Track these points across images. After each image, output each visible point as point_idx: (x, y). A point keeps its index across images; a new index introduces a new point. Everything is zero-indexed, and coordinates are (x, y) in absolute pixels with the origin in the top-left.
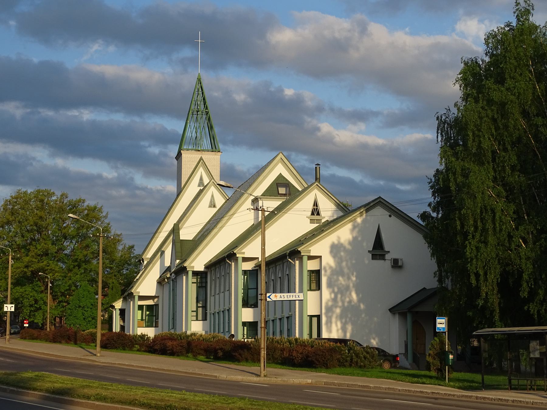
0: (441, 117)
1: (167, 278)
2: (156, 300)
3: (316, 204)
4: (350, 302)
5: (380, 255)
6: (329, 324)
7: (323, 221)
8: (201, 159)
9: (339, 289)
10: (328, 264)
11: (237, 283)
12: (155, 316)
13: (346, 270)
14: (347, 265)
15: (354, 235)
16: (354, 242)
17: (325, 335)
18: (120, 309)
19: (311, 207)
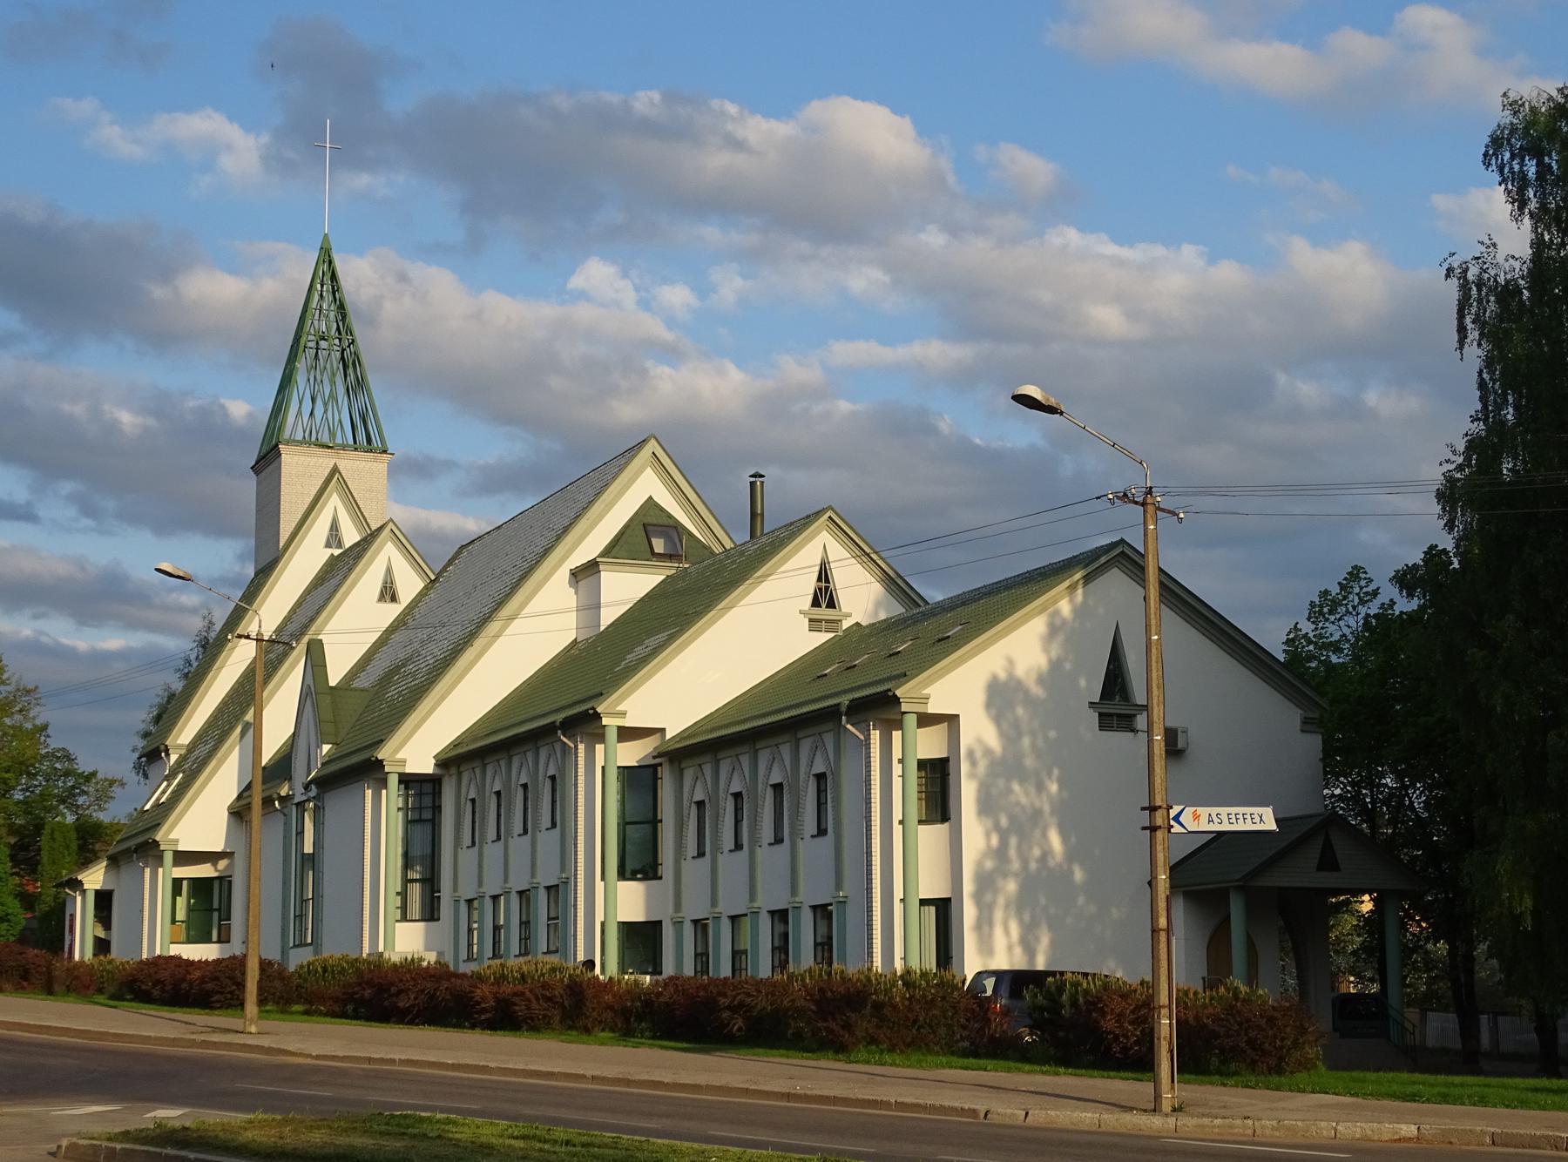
0: (1466, 271)
1: (282, 799)
2: (222, 864)
3: (824, 575)
4: (1046, 855)
5: (1119, 715)
6: (986, 928)
7: (846, 624)
8: (335, 470)
9: (1012, 818)
10: (979, 740)
11: (596, 805)
12: (219, 910)
13: (1029, 762)
14: (1033, 745)
15: (1054, 654)
16: (1053, 676)
17: (972, 963)
18: (97, 892)
19: (810, 583)
